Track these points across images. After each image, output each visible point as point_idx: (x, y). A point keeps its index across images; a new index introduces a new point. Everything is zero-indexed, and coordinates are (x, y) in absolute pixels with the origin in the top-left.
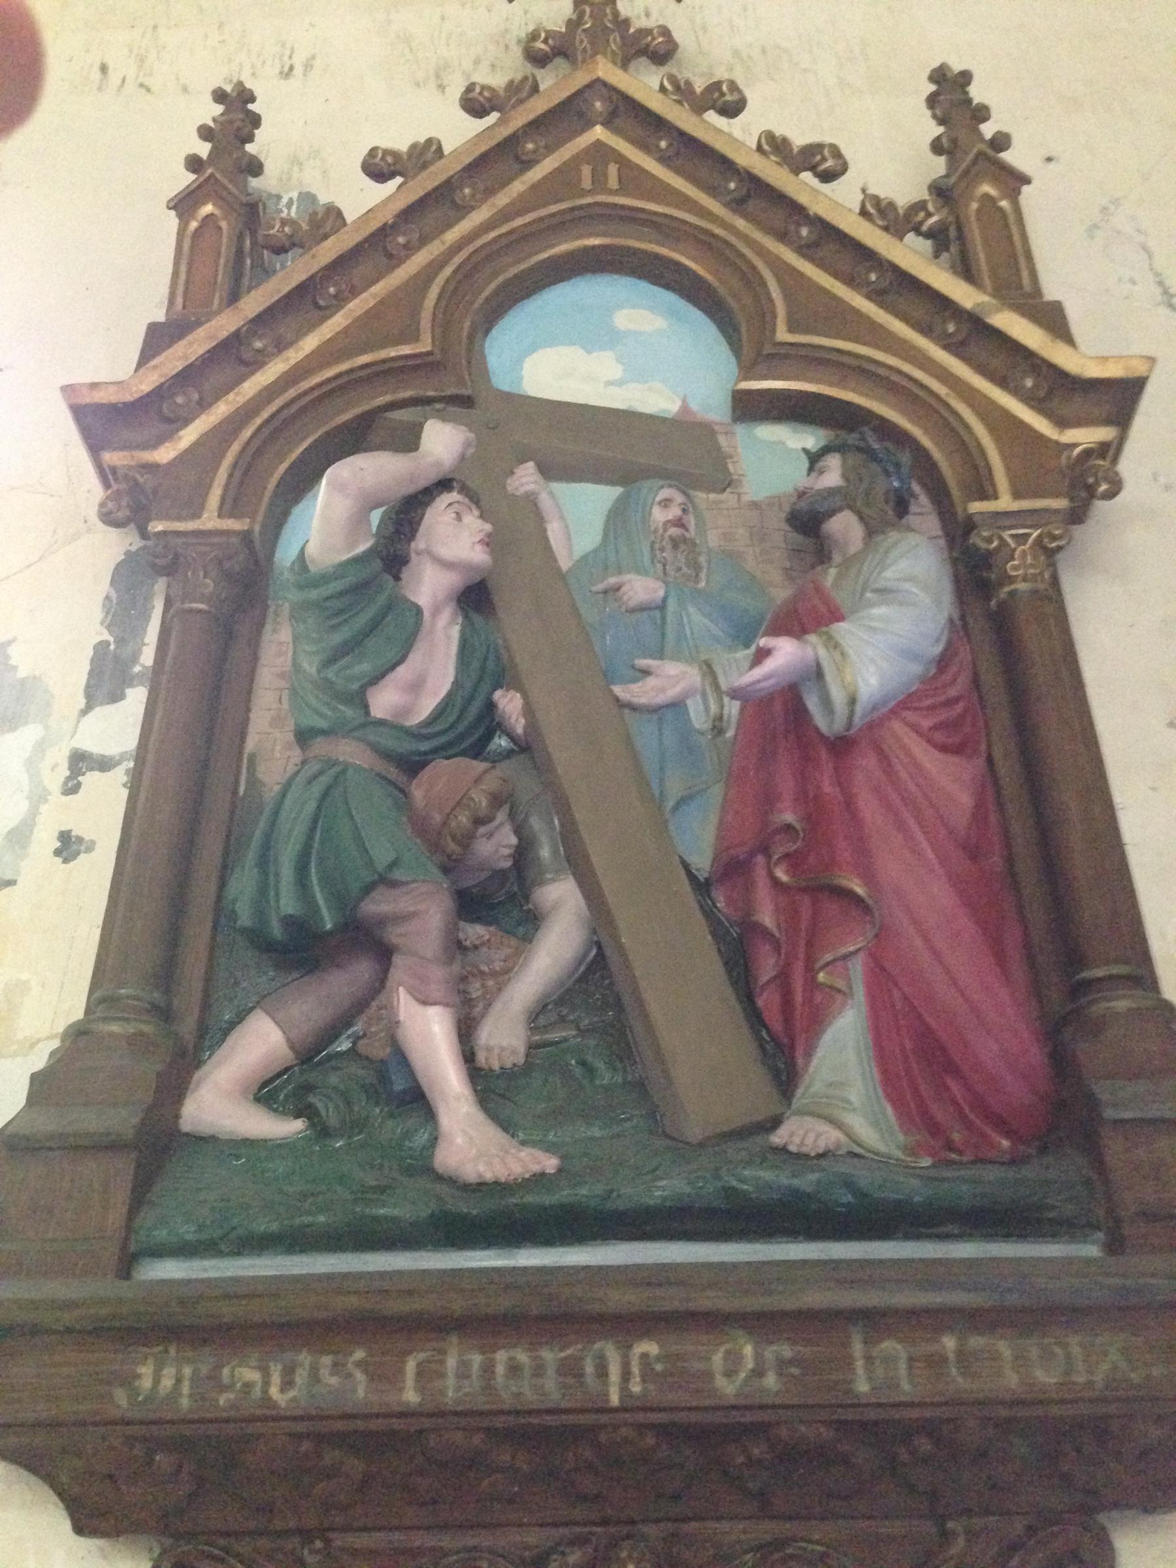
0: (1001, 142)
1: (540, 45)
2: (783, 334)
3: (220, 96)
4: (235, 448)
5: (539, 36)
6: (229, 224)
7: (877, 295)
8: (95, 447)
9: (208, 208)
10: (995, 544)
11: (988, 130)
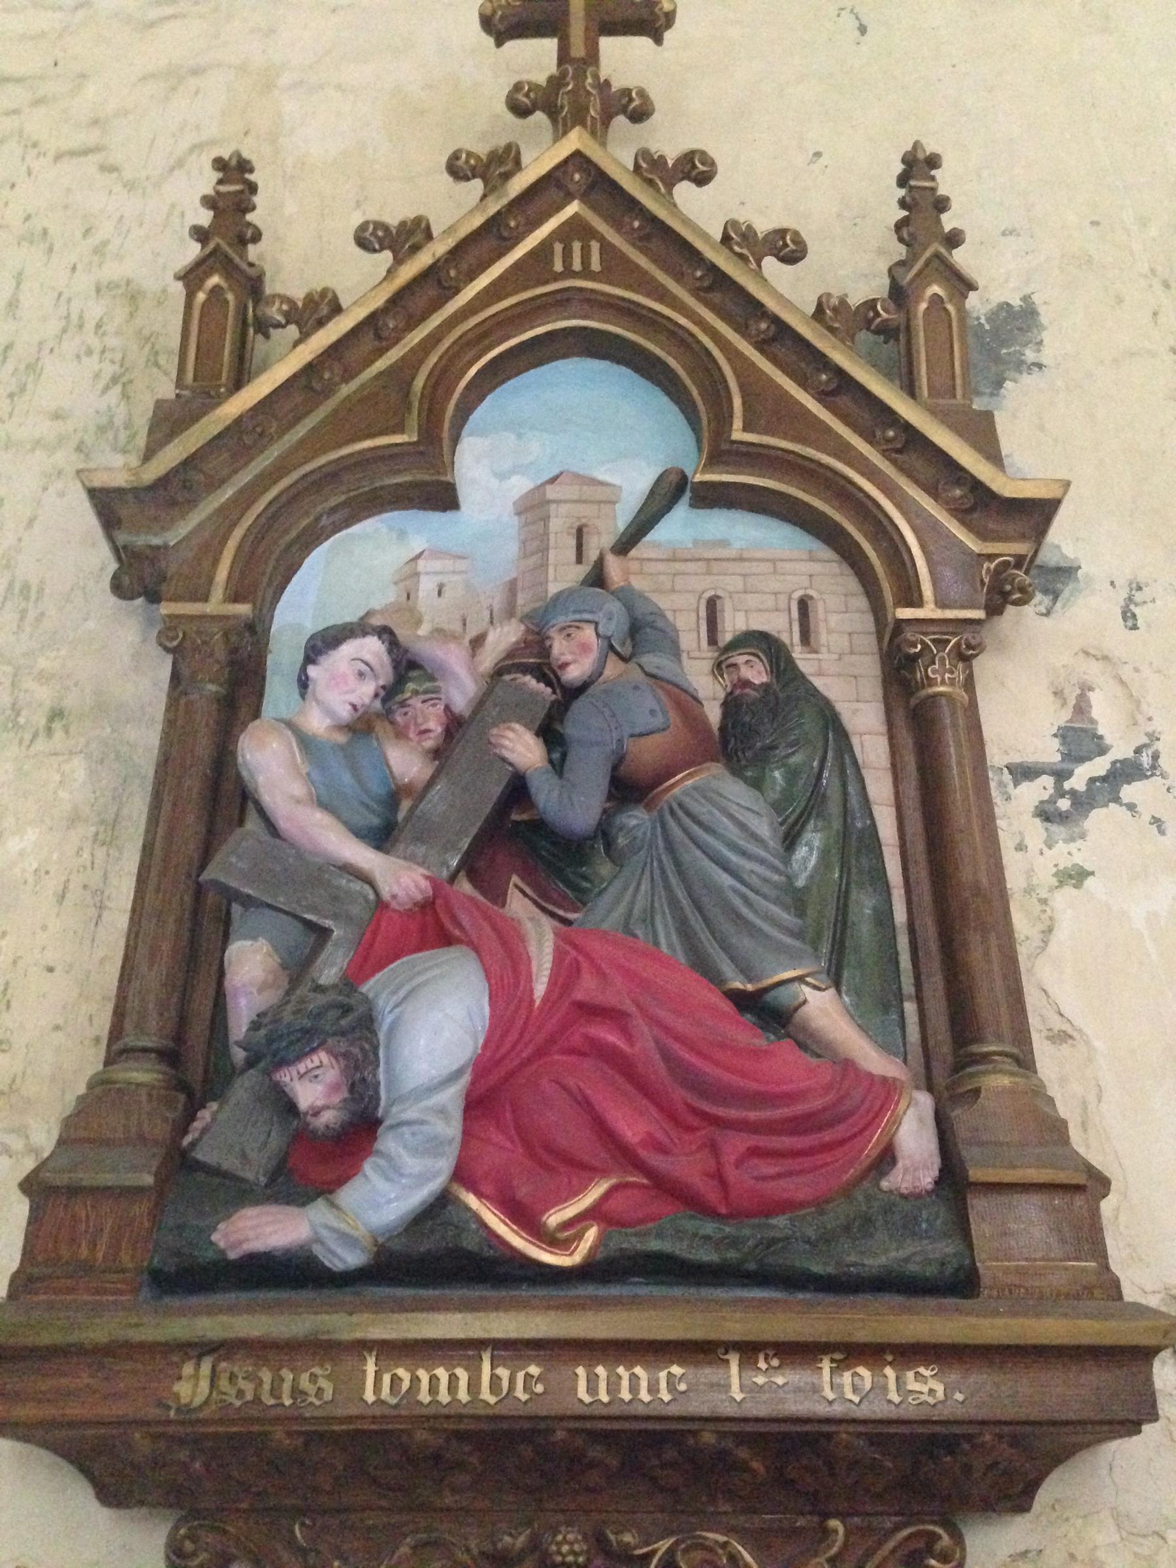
1: (521, 97)
2: (738, 434)
4: (238, 533)
5: (522, 88)
6: (236, 298)
7: (823, 396)
9: (215, 280)
10: (919, 646)
11: (949, 221)
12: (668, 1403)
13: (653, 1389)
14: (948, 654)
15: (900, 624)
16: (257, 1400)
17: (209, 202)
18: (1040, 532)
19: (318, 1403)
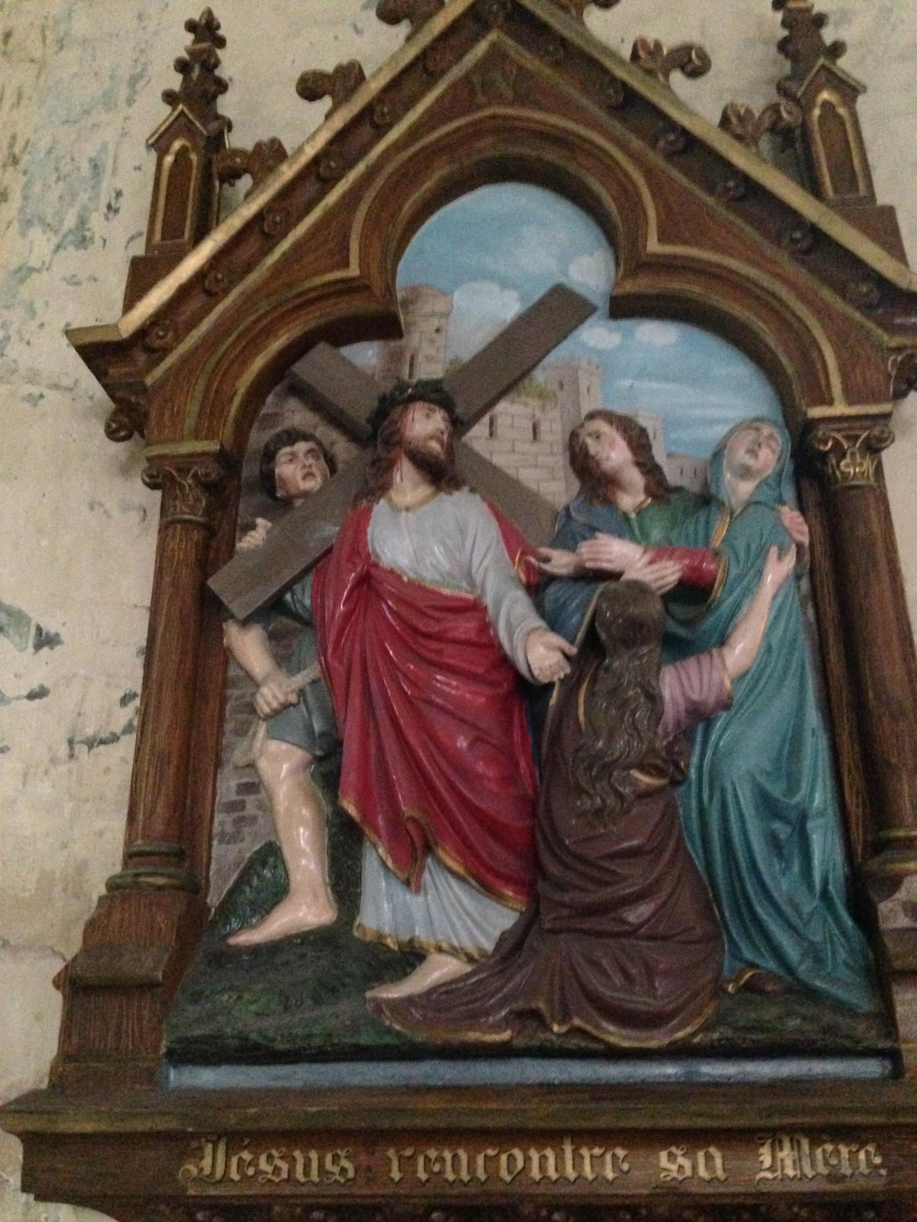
0: (837, 49)
2: (653, 245)
3: (191, 26)
9: (177, 145)
10: (830, 444)
11: (828, 35)
12: (511, 1182)
14: (860, 448)
15: (812, 425)
16: (290, 1179)
17: (182, 66)
19: (342, 1180)
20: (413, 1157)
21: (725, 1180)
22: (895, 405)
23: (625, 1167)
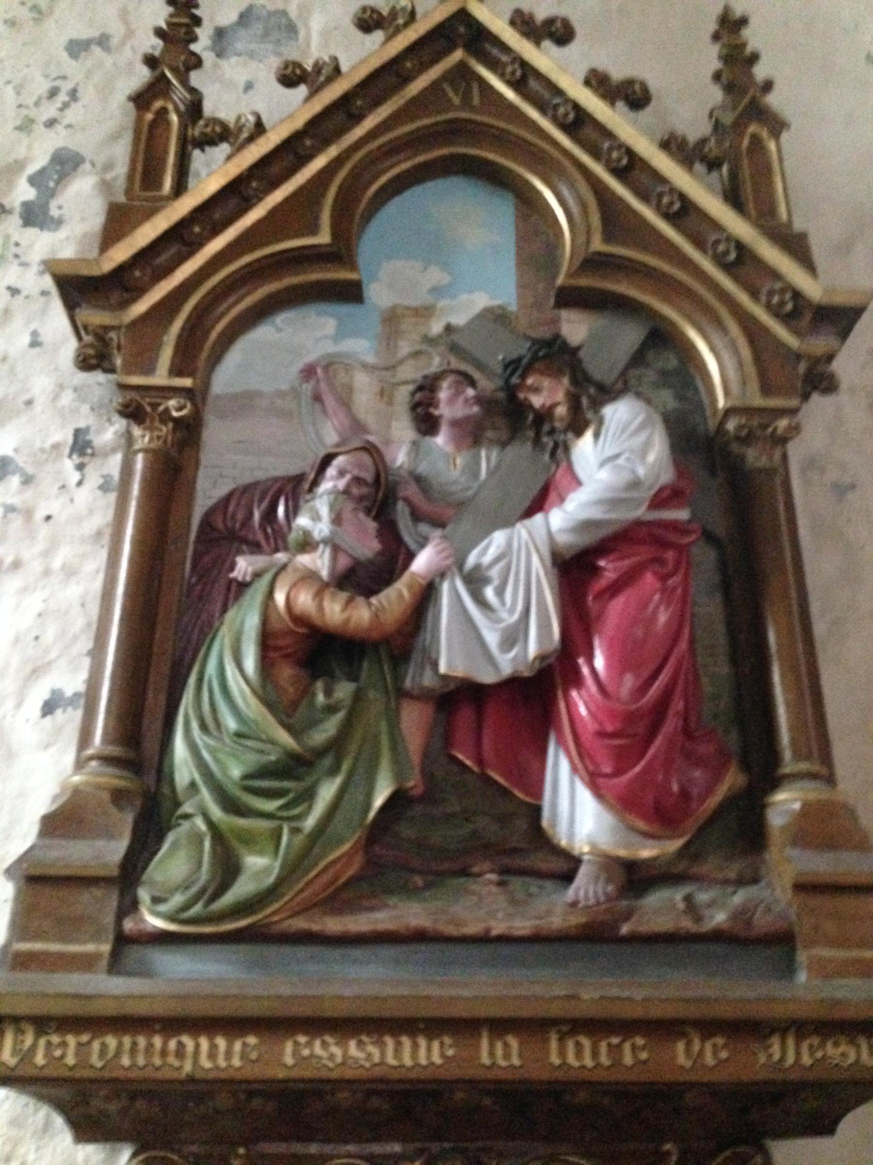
2: (324, 237)
8: (70, 306)
11: (760, 72)
13: (229, 1054)
18: (844, 334)
20: (619, 1046)
21: (692, 1067)
22: (802, 403)
23: (724, 1055)
